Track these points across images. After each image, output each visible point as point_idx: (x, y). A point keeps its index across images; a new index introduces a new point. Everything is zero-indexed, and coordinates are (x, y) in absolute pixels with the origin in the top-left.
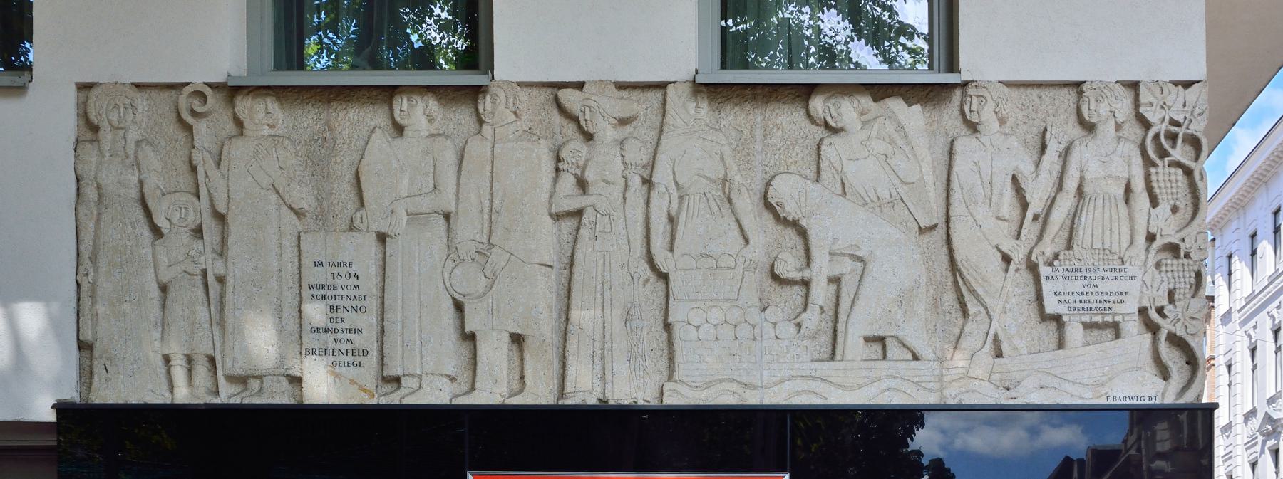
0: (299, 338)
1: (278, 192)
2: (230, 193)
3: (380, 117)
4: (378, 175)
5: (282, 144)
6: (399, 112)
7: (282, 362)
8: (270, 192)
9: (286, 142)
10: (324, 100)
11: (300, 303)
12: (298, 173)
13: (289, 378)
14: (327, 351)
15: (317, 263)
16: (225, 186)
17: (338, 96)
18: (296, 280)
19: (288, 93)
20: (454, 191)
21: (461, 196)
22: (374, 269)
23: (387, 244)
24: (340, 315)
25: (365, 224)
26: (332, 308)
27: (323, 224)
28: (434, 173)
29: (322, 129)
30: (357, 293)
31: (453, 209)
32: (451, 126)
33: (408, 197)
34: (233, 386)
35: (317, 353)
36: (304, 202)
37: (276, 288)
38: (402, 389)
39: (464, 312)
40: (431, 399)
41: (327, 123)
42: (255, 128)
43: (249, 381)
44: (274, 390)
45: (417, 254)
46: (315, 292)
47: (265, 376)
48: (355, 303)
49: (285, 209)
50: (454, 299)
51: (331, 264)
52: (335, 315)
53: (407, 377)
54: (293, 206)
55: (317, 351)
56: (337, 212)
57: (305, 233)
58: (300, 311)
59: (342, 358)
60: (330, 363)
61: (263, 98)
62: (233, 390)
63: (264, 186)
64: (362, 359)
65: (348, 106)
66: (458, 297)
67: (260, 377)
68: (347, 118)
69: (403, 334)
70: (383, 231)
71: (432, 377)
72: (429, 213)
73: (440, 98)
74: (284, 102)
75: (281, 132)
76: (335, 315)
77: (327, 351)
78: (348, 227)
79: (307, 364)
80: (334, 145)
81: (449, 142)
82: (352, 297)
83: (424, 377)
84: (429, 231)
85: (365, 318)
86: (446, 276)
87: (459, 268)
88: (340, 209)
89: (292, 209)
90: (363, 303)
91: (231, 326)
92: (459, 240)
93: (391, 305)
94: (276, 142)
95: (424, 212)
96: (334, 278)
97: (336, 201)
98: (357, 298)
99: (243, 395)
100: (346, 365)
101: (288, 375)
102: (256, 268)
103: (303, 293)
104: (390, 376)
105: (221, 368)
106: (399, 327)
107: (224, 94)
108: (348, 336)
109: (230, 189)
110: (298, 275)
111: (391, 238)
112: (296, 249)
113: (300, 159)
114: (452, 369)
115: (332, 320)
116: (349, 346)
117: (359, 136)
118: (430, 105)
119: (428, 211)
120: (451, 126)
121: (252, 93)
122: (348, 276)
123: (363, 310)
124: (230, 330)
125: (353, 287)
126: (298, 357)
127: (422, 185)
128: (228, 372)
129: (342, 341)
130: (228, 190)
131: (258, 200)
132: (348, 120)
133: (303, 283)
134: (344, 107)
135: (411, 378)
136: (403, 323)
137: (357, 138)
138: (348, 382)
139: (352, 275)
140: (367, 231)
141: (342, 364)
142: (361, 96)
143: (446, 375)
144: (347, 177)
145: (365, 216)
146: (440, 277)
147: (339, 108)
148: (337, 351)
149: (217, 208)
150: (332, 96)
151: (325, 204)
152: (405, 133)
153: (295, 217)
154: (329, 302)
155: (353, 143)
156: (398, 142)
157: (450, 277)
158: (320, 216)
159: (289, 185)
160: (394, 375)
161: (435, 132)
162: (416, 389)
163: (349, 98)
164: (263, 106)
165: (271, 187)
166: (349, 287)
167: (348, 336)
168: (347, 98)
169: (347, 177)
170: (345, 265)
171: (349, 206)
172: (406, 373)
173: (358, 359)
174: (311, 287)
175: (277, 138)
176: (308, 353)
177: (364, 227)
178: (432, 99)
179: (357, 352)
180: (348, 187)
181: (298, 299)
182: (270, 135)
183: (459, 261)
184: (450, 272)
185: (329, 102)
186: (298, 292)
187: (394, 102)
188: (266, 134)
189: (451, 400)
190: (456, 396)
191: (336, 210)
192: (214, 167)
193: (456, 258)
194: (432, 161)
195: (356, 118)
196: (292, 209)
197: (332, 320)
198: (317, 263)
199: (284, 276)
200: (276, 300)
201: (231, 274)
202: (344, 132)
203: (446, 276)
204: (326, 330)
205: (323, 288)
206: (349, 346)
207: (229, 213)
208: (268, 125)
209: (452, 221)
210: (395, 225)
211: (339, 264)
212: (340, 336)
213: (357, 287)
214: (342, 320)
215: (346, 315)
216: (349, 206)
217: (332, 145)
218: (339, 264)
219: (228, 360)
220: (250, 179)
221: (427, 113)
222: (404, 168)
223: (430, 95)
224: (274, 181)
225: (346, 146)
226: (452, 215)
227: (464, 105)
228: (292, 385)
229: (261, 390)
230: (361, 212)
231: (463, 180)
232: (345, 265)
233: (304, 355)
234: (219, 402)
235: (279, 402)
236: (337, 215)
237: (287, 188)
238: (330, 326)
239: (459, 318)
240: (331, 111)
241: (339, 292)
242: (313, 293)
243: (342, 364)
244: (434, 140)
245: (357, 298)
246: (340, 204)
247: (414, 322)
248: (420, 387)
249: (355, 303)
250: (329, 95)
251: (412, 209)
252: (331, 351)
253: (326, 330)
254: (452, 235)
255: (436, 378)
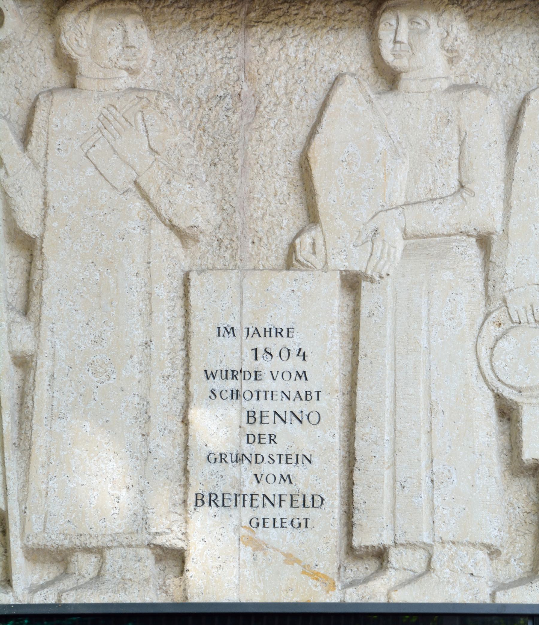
0: (181, 473)
1: (145, 197)
2: (49, 196)
3: (349, 55)
4: (348, 164)
5: (157, 106)
6: (391, 45)
7: (145, 520)
8: (129, 195)
9: (164, 103)
10: (237, 23)
11: (187, 406)
12: (186, 160)
13: (159, 551)
14: (240, 499)
15: (222, 330)
16: (39, 182)
17: (266, 14)
18: (179, 362)
19: (165, 10)
20: (500, 191)
21: (514, 202)
22: (337, 341)
23: (363, 293)
24: (266, 430)
25: (321, 255)
26: (251, 417)
27: (232, 257)
28: (460, 159)
29: (233, 76)
30: (302, 386)
31: (498, 227)
32: (492, 68)
33: (407, 204)
34: (39, 567)
35: (220, 503)
36: (197, 214)
37: (138, 376)
38: (391, 573)
39: (518, 421)
40: (451, 592)
41: (244, 67)
42: (101, 75)
43: (74, 559)
44: (128, 576)
45: (424, 313)
46: (217, 384)
47: (109, 548)
48: (297, 406)
49: (159, 229)
50: (498, 397)
51: (251, 331)
52: (256, 429)
53: (401, 549)
54: (176, 222)
55: (220, 498)
56: (261, 234)
57: (201, 271)
58: (185, 422)
59: (269, 512)
60: (246, 522)
61: (119, 17)
62: (36, 577)
63: (118, 184)
64: (310, 513)
65: (284, 33)
66: (507, 393)
67: (99, 551)
68: (283, 56)
69: (394, 464)
70: (357, 269)
71: (454, 548)
72: (450, 235)
73: (471, 17)
74: (156, 25)
75: (149, 82)
76: (256, 429)
77: (240, 499)
78: (281, 262)
79: (198, 524)
80: (257, 108)
81: (491, 99)
82: (293, 395)
83: (437, 551)
84: (448, 269)
85: (319, 433)
86: (484, 353)
87: (511, 338)
88: (267, 227)
89: (172, 227)
90: (313, 405)
91: (43, 451)
92: (510, 284)
93: (369, 410)
94: (144, 102)
95: (441, 232)
96: (256, 359)
97: (260, 213)
98: (303, 395)
99: (61, 586)
100: (278, 524)
101: (157, 546)
102: (98, 340)
103: (194, 387)
104: (367, 547)
105: (17, 533)
106: (387, 452)
107: (35, 9)
108: (283, 469)
109: (50, 189)
110: (183, 354)
111: (372, 280)
112: (180, 303)
113: (188, 133)
114: (496, 533)
115: (251, 438)
116: (284, 489)
117: (306, 91)
118: (455, 30)
119: (447, 230)
120: (492, 68)
121: (96, 9)
122: (285, 354)
123: (314, 418)
124: (42, 459)
125: (294, 375)
126: (180, 510)
127: (434, 181)
128: (33, 542)
129: (271, 479)
130: (46, 192)
131: (106, 211)
132: (287, 61)
133: (193, 369)
134: (278, 36)
135: (410, 552)
136: (395, 443)
137: (302, 93)
138: (282, 558)
139: (294, 353)
140: (325, 268)
141: (270, 523)
142: (311, 14)
143: (483, 545)
144: (282, 167)
145: (320, 242)
146: (471, 356)
147: (268, 37)
148: (260, 498)
149: (20, 225)
150: (253, 15)
151: (238, 219)
152: (403, 84)
153: (176, 242)
154: (245, 404)
155: (295, 103)
156: (390, 99)
157: (492, 355)
158: (226, 242)
159: (169, 183)
160: (375, 544)
161: (459, 81)
162: (419, 571)
163: (288, 19)
164: (118, 33)
165: (131, 186)
166: (286, 376)
167: (283, 469)
168: (283, 20)
169: (282, 167)
170: (279, 333)
171: (285, 222)
172: (401, 540)
173: (303, 513)
174: (210, 375)
175: (145, 95)
176: (200, 503)
177: (317, 261)
178: (458, 18)
179: (301, 500)
180: (283, 187)
181: (181, 397)
182: (132, 89)
183: (509, 324)
184: (491, 344)
185: (248, 27)
186: (182, 384)
187: (382, 26)
188: (123, 87)
189: (493, 595)
190: (504, 587)
191: (259, 229)
192: (17, 147)
193: (504, 318)
194: (456, 137)
195: (301, 56)
196: (172, 227)
197: (251, 438)
198: (222, 330)
199: (154, 355)
200: (137, 399)
201: (47, 350)
202: (276, 83)
203: (484, 353)
204: (239, 458)
205: (234, 377)
206: (284, 489)
207: (47, 234)
208: (127, 69)
209: (495, 248)
210: (381, 258)
211: (268, 332)
212: (266, 468)
213: (302, 375)
214: (272, 439)
215: (279, 428)
216: (285, 222)
217: (253, 108)
218: (268, 332)
219: (34, 517)
220: (90, 171)
221: (447, 45)
222: (400, 150)
223: (456, 10)
224: (139, 176)
225: (281, 110)
226: (494, 237)
227: (520, 29)
228: (161, 566)
229: (99, 575)
230: (313, 233)
231: (519, 170)
232: (279, 333)
233: (192, 507)
234: (12, 602)
235: (138, 601)
236: (260, 240)
237: (165, 189)
238: (247, 449)
239: (503, 433)
240: (250, 42)
241: (267, 384)
242: (215, 387)
243: (270, 523)
244: (461, 97)
245: (303, 395)
246: (267, 217)
247: (418, 440)
248: (429, 568)
249: (297, 406)
250: (247, 13)
251: (414, 226)
252: (248, 498)
253: (239, 458)
254: (495, 274)
255: (462, 551)
